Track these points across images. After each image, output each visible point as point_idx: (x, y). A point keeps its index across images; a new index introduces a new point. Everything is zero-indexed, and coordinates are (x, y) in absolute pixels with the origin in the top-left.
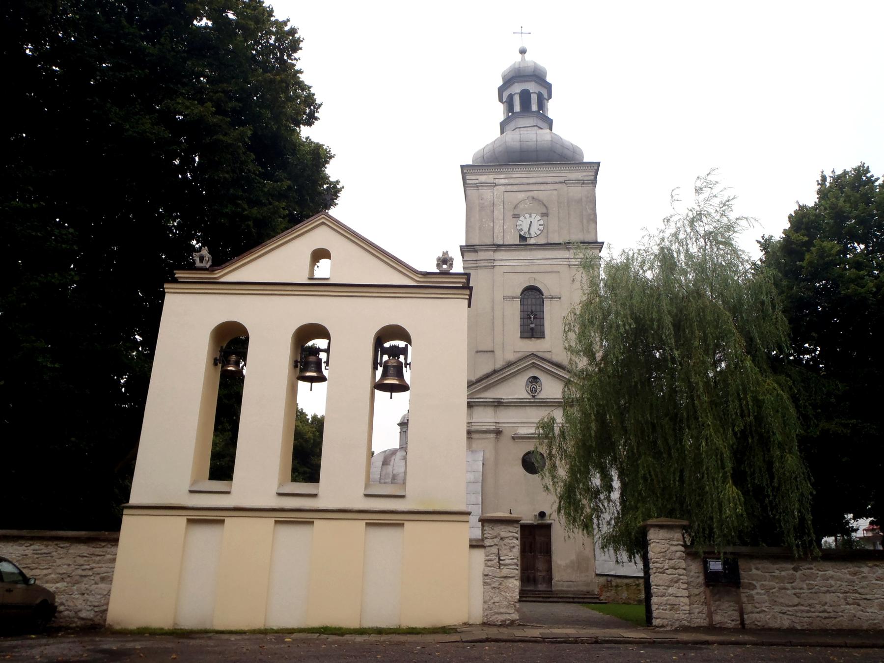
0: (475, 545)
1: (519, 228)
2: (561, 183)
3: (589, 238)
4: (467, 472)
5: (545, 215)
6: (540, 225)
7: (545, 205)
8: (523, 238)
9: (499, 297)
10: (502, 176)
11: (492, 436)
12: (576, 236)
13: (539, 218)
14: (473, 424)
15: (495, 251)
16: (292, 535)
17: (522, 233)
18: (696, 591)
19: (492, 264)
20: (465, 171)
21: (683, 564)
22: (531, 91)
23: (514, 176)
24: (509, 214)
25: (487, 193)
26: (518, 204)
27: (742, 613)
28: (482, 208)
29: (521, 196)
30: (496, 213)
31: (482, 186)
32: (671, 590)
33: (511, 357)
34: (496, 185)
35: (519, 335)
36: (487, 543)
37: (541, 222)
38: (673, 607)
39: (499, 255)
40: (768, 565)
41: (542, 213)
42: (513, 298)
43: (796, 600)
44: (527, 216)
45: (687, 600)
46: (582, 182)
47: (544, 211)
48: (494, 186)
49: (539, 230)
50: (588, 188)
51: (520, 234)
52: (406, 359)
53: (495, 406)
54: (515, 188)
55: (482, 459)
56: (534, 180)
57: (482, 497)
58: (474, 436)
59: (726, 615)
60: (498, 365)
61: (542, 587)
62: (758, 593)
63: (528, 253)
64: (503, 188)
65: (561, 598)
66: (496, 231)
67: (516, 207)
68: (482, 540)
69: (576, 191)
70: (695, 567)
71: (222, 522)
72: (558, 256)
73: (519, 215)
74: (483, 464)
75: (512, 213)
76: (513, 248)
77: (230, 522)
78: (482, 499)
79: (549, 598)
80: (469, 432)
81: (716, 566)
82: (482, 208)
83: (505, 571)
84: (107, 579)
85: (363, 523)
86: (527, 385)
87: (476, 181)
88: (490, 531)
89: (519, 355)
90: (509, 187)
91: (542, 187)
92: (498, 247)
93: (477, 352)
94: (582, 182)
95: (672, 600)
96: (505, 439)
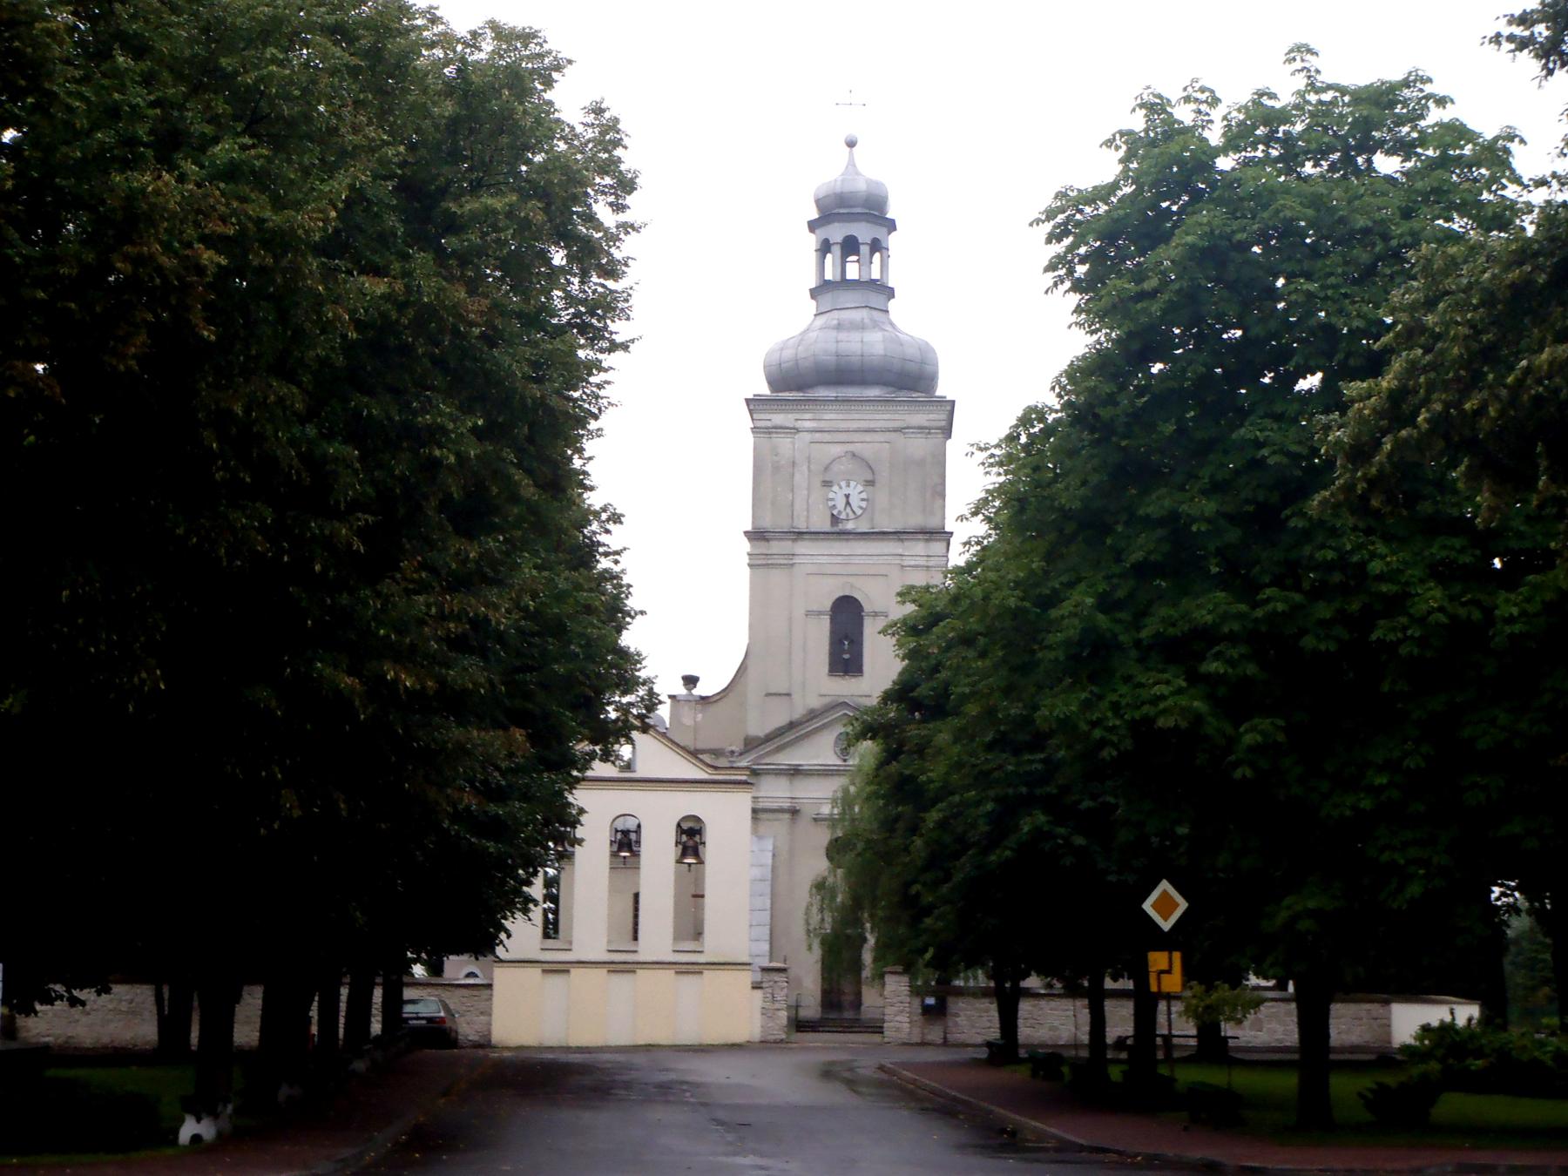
0: (757, 986)
1: (831, 503)
2: (895, 430)
3: (932, 523)
4: (752, 865)
5: (870, 483)
6: (863, 500)
7: (870, 468)
8: (835, 519)
9: (799, 612)
10: (808, 416)
11: (787, 816)
12: (915, 520)
13: (860, 488)
14: (760, 800)
15: (794, 540)
16: (622, 982)
17: (835, 512)
18: (915, 1018)
19: (791, 562)
20: (752, 407)
21: (908, 999)
22: (860, 241)
23: (826, 417)
24: (817, 482)
25: (784, 443)
26: (831, 463)
27: (945, 1033)
28: (776, 468)
29: (837, 450)
30: (797, 477)
31: (776, 433)
32: (898, 1018)
33: (815, 702)
34: (797, 430)
35: (826, 668)
36: (764, 985)
37: (864, 495)
38: (898, 1030)
39: (803, 547)
40: (971, 1000)
41: (866, 481)
42: (820, 613)
43: (989, 1025)
44: (843, 484)
45: (908, 1025)
46: (923, 430)
47: (870, 477)
48: (795, 433)
49: (861, 508)
50: (936, 439)
51: (833, 515)
52: (701, 839)
53: (793, 775)
54: (827, 437)
55: (771, 848)
56: (855, 425)
57: (772, 899)
58: (763, 816)
59: (935, 1034)
60: (797, 714)
61: (848, 1014)
62: (961, 1020)
63: (844, 544)
64: (807, 437)
65: (847, 1027)
66: (797, 507)
67: (827, 469)
68: (762, 982)
69: (918, 446)
70: (917, 1002)
71: (568, 971)
72: (886, 551)
73: (831, 482)
74: (774, 855)
75: (822, 479)
76: (822, 536)
77: (576, 972)
78: (772, 904)
79: (852, 1027)
80: (755, 811)
81: (931, 1001)
82: (776, 468)
83: (777, 1006)
84: (488, 1013)
85: (673, 971)
86: (836, 743)
87: (769, 424)
88: (767, 977)
89: (826, 700)
90: (818, 435)
91: (868, 437)
92: (799, 535)
93: (768, 695)
94: (923, 430)
95: (898, 1025)
96: (804, 823)
